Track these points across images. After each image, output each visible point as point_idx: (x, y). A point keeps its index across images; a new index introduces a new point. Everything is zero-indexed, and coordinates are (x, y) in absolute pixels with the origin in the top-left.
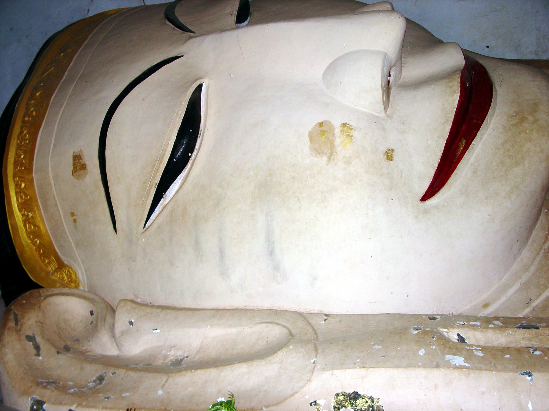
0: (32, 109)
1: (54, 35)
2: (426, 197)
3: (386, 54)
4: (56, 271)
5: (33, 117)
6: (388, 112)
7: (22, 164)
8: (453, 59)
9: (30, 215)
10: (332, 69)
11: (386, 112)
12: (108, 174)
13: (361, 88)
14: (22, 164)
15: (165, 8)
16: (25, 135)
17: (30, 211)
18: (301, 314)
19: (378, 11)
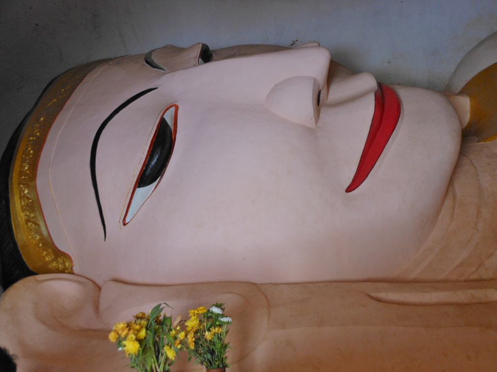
0: (36, 131)
1: (103, 122)
2: (350, 189)
3: (315, 80)
4: (53, 261)
5: (37, 137)
6: (318, 125)
7: (26, 175)
8: (367, 83)
9: (32, 215)
10: (277, 89)
11: (316, 125)
12: (135, 194)
13: (298, 106)
14: (26, 175)
15: (144, 57)
16: (30, 151)
17: (32, 213)
18: (254, 284)
19: (306, 47)
